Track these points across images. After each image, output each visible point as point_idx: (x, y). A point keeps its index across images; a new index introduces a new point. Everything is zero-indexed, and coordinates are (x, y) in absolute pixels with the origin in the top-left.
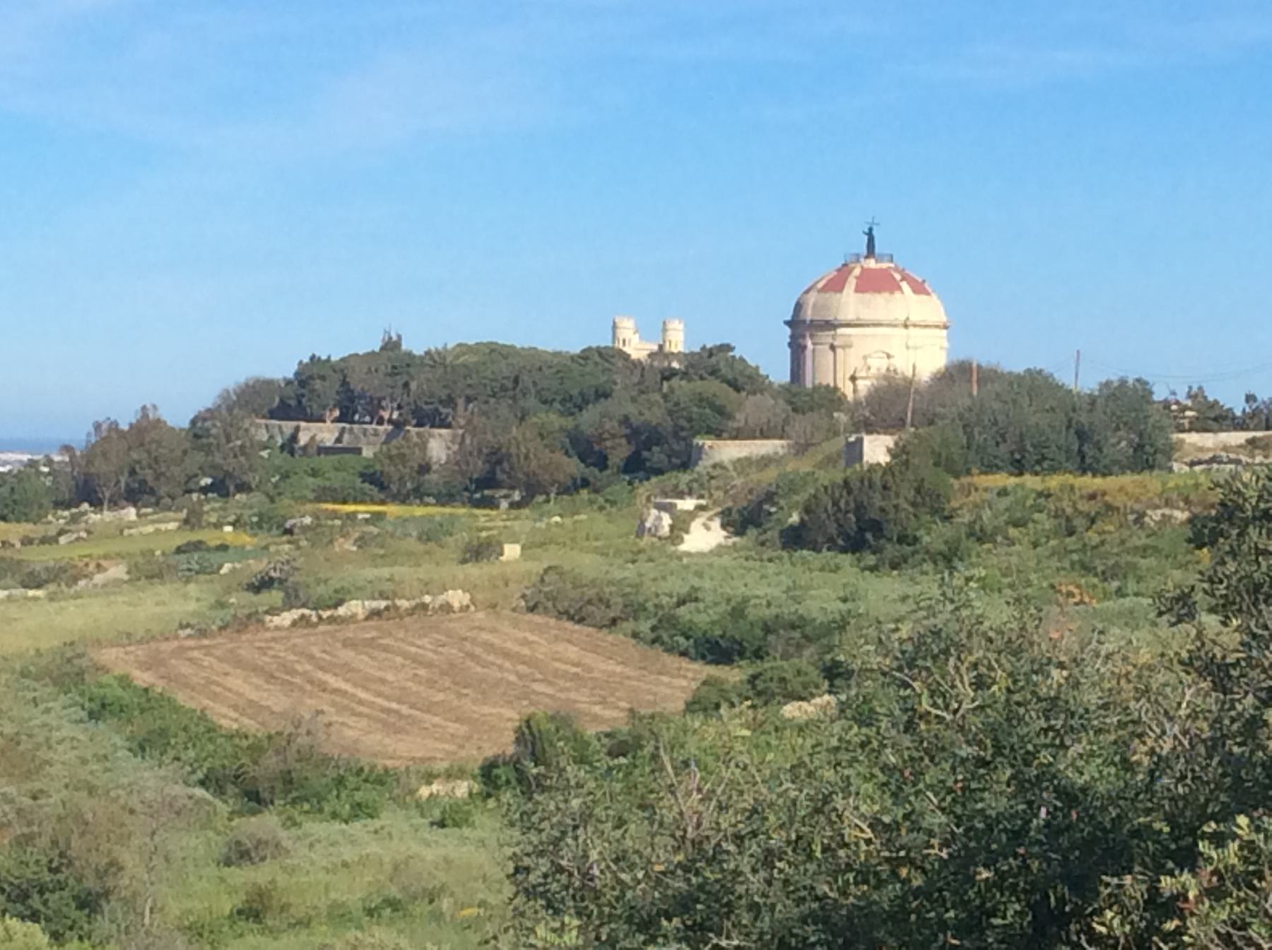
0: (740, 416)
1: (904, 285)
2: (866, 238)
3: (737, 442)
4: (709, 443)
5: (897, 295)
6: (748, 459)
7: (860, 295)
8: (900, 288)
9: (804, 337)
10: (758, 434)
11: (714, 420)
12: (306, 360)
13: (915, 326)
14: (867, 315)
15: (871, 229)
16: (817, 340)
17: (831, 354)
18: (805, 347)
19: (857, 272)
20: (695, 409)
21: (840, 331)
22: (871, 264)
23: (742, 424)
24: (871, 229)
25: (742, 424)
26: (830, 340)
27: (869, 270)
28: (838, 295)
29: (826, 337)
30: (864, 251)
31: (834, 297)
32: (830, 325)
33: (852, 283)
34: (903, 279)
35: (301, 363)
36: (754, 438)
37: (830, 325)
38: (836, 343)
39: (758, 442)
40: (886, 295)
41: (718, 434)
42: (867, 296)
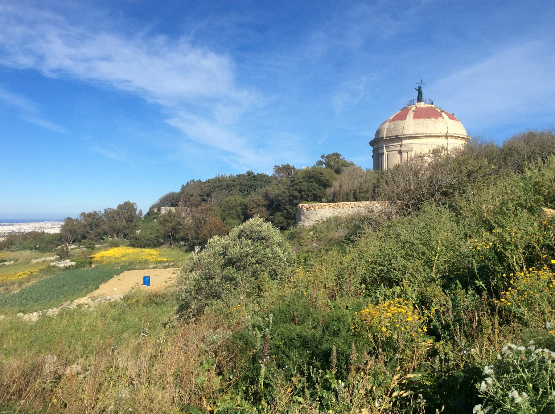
0: (336, 184)
1: (443, 114)
2: (416, 93)
3: (332, 204)
4: (306, 205)
5: (440, 119)
6: (336, 219)
7: (415, 120)
8: (441, 116)
9: (382, 148)
10: (351, 196)
11: (318, 192)
12: (185, 184)
13: (452, 136)
14: (421, 131)
15: (420, 88)
16: (390, 149)
17: (399, 156)
18: (383, 154)
19: (414, 108)
20: (306, 183)
21: (404, 142)
22: (422, 105)
23: (338, 189)
24: (420, 88)
25: (338, 189)
26: (398, 148)
27: (421, 108)
28: (403, 121)
29: (396, 146)
30: (416, 97)
31: (400, 123)
32: (398, 139)
33: (411, 114)
34: (442, 111)
35: (183, 185)
36: (347, 200)
37: (398, 139)
38: (402, 149)
39: (351, 204)
40: (433, 119)
41: (317, 198)
42: (422, 120)
